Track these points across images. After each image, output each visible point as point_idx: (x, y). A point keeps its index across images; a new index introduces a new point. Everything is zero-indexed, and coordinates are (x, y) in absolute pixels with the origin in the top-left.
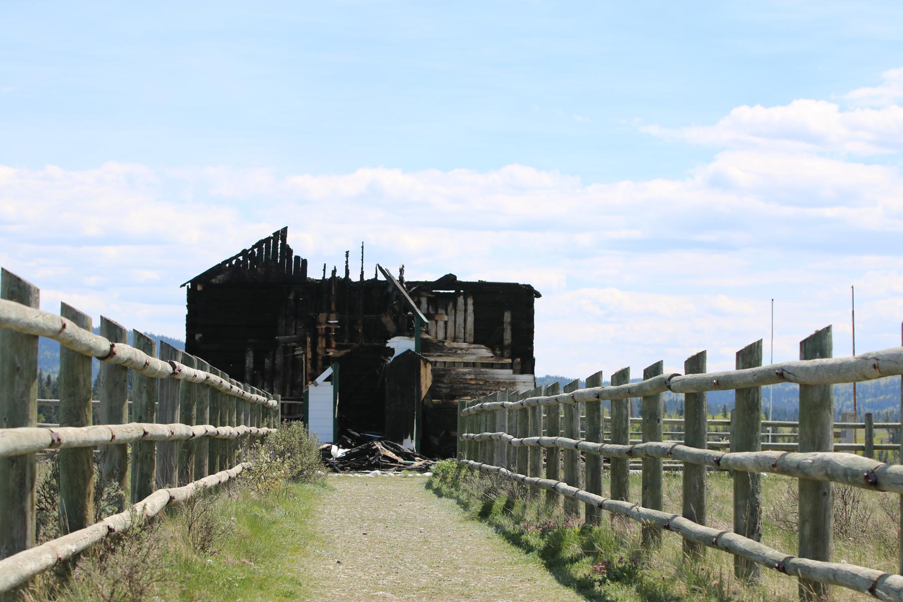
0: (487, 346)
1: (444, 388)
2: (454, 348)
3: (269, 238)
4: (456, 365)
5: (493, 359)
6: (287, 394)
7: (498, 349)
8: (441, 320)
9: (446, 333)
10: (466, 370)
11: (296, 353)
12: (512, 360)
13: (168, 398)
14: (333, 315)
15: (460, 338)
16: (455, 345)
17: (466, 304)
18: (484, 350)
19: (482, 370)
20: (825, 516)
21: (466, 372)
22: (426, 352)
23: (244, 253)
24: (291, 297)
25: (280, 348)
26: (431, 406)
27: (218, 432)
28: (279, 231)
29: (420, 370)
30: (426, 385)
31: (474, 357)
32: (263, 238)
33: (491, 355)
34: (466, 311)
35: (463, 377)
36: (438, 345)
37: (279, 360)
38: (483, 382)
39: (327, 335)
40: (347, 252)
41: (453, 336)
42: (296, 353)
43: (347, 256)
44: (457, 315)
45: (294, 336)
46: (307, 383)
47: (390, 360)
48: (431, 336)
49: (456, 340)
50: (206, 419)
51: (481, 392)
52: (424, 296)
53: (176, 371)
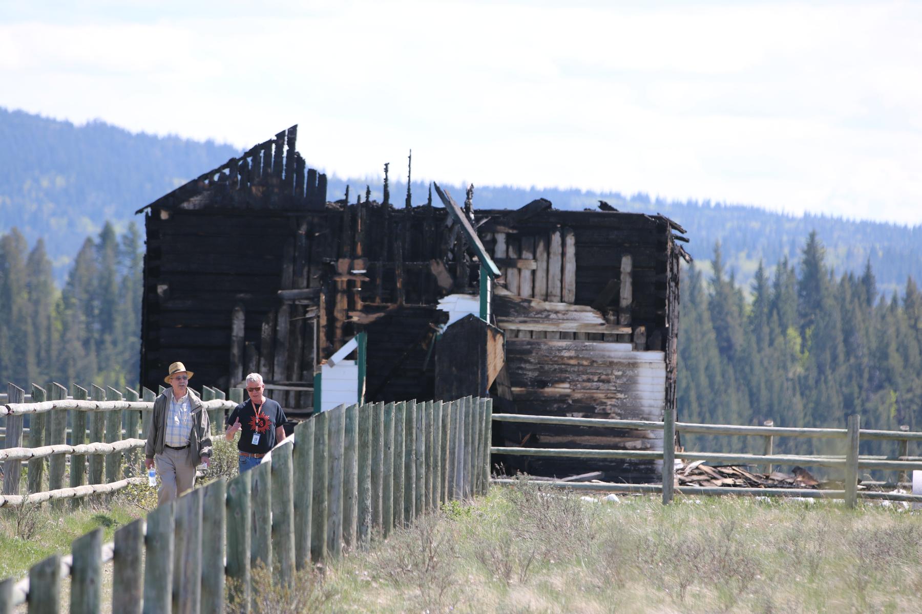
0: (595, 309)
1: (530, 370)
2: (546, 310)
3: (270, 142)
4: (548, 336)
5: (604, 327)
6: (295, 377)
7: (611, 312)
8: (527, 268)
9: (533, 288)
10: (563, 343)
11: (308, 315)
12: (633, 330)
13: (13, 427)
14: (359, 262)
15: (555, 296)
16: (547, 305)
17: (563, 244)
18: (591, 313)
19: (587, 344)
20: (350, 510)
21: (562, 347)
22: (503, 316)
23: (232, 163)
24: (303, 231)
25: (285, 307)
26: (509, 397)
27: (74, 450)
28: (284, 132)
29: (486, 344)
30: (495, 366)
31: (576, 325)
32: (261, 142)
33: (601, 321)
34: (563, 254)
35: (558, 354)
36: (522, 306)
37: (283, 324)
38: (588, 361)
39: (349, 290)
40: (386, 165)
41: (544, 292)
42: (308, 315)
43: (386, 170)
44: (551, 261)
45: (306, 290)
46: (319, 362)
47: (442, 328)
48: (511, 291)
49: (549, 298)
50: (64, 439)
51: (585, 377)
52: (501, 232)
53: (10, 412)
